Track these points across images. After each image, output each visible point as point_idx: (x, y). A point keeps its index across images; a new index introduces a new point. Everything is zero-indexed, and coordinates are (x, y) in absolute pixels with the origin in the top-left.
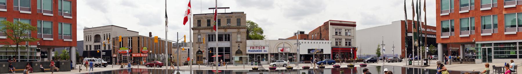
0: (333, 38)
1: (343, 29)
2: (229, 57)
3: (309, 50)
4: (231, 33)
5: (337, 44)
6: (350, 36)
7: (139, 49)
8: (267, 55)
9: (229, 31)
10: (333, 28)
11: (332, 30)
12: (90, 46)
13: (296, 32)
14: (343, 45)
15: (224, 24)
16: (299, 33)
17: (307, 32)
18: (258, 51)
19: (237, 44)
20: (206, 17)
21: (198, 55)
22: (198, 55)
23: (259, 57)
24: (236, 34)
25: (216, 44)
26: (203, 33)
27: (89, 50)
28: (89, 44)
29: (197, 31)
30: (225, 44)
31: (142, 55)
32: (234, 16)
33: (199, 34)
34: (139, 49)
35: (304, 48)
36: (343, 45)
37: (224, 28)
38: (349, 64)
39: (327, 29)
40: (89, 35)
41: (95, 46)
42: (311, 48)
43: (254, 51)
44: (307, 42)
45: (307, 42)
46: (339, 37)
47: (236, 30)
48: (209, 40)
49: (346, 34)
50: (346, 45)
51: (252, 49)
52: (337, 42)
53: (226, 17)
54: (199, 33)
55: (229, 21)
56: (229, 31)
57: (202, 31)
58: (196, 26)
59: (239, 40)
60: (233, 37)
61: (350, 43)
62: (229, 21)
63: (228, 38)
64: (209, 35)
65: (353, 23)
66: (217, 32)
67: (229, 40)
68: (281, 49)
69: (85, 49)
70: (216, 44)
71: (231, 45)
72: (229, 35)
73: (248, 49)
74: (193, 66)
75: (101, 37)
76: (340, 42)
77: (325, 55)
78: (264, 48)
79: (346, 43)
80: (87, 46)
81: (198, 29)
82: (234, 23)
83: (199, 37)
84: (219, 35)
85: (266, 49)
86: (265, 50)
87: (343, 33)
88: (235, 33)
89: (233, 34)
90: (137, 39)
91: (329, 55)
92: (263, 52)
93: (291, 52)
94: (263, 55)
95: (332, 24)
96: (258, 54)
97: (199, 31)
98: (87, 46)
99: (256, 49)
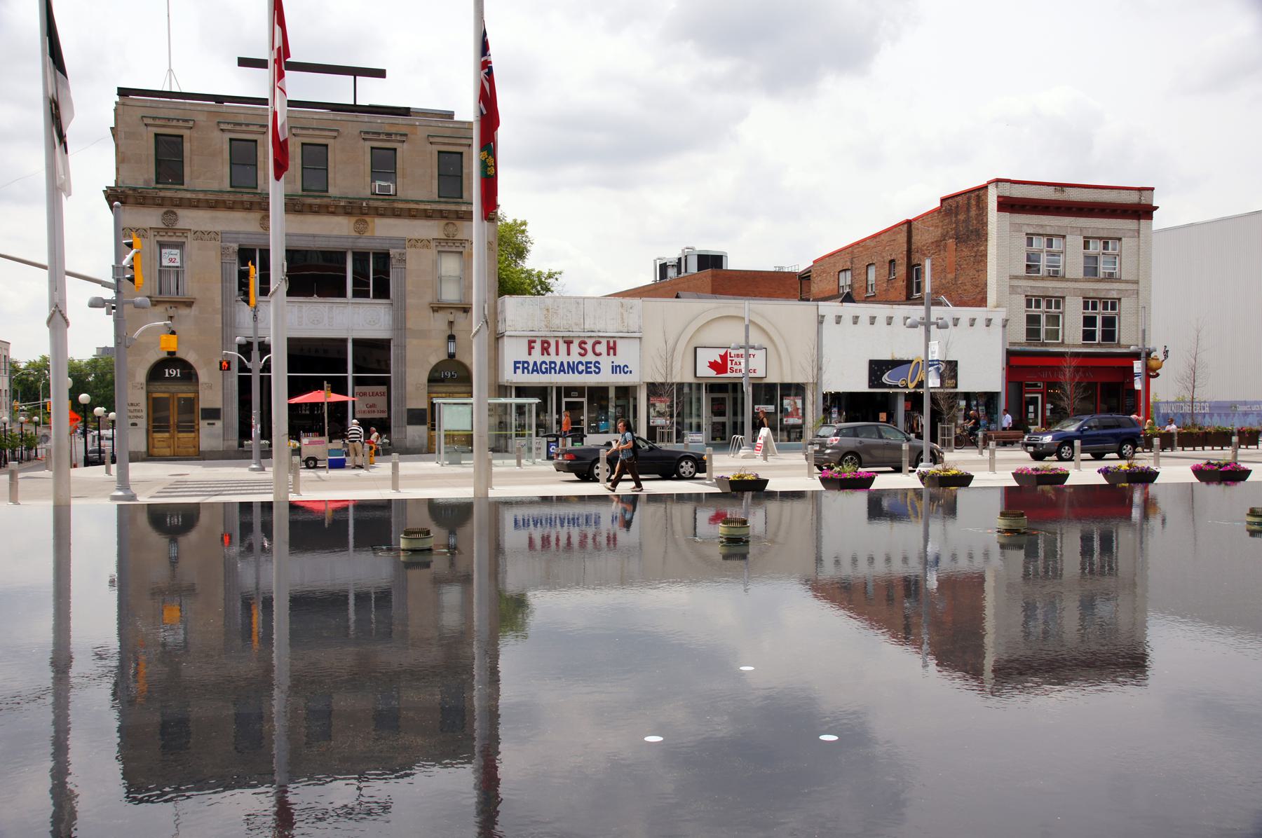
0: (1013, 290)
1: (1072, 243)
2: (381, 402)
3: (877, 368)
4: (403, 242)
5: (1032, 333)
6: (1110, 277)
8: (625, 393)
9: (384, 230)
10: (1016, 228)
11: (1003, 239)
13: (672, 255)
14: (1071, 335)
15: (349, 175)
16: (693, 267)
17: (732, 264)
18: (573, 368)
19: (439, 323)
20: (221, 124)
21: (161, 392)
22: (161, 392)
23: (574, 408)
24: (431, 253)
25: (284, 319)
26: (201, 235)
27: (109, 294)
29: (151, 218)
30: (347, 319)
32: (422, 133)
33: (169, 237)
35: (844, 348)
36: (1071, 335)
37: (353, 208)
38: (1113, 462)
39: (974, 235)
42: (886, 356)
43: (551, 368)
44: (964, 321)
45: (964, 321)
46: (1052, 287)
47: (430, 230)
49: (1091, 270)
50: (1089, 336)
51: (537, 356)
52: (1033, 320)
53: (366, 135)
54: (169, 228)
55: (384, 163)
56: (384, 230)
57: (189, 219)
58: (144, 175)
60: (412, 273)
61: (1109, 322)
62: (384, 163)
63: (375, 275)
64: (245, 255)
65: (1132, 198)
66: (280, 232)
67: (382, 291)
68: (715, 356)
70: (284, 319)
71: (400, 323)
72: (383, 259)
73: (513, 351)
74: (138, 471)
76: (1054, 319)
77: (967, 396)
78: (612, 349)
79: (1090, 321)
81: (159, 202)
82: (417, 179)
83: (171, 257)
84: (291, 254)
85: (627, 353)
86: (619, 360)
87: (1073, 263)
88: (425, 243)
89: (410, 253)
91: (991, 398)
92: (605, 377)
93: (773, 378)
94: (598, 394)
95: (1007, 205)
96: (569, 390)
97: (170, 216)
99: (563, 358)
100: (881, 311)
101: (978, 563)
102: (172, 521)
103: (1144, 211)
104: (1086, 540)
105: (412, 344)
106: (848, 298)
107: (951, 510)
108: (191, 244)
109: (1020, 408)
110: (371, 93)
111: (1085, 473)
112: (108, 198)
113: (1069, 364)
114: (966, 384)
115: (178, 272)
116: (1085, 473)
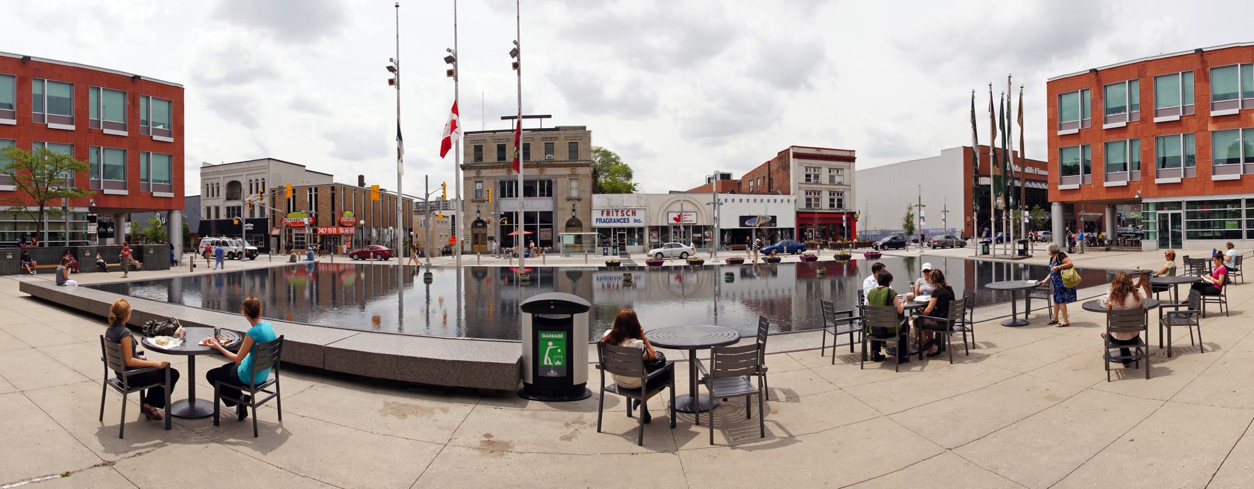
1: (824, 168)
2: (549, 234)
3: (743, 219)
4: (556, 176)
6: (840, 184)
7: (333, 215)
8: (641, 230)
9: (550, 172)
10: (801, 165)
11: (797, 170)
12: (217, 209)
13: (712, 174)
14: (825, 205)
15: (537, 154)
16: (719, 178)
17: (737, 176)
18: (619, 221)
19: (569, 205)
20: (494, 140)
21: (476, 231)
22: (476, 231)
23: (622, 236)
25: (519, 204)
26: (488, 178)
28: (213, 203)
29: (473, 173)
30: (540, 204)
31: (341, 230)
33: (479, 180)
34: (333, 215)
35: (730, 213)
36: (825, 205)
37: (539, 165)
38: (838, 252)
39: (786, 167)
40: (215, 182)
41: (228, 208)
43: (610, 221)
46: (816, 187)
48: (503, 195)
49: (832, 179)
50: (832, 206)
51: (605, 217)
52: (808, 200)
53: (543, 139)
55: (549, 148)
56: (550, 172)
57: (484, 173)
58: (471, 159)
59: (574, 194)
60: (560, 187)
61: (840, 201)
62: (549, 148)
63: (547, 189)
64: (502, 183)
65: (847, 154)
66: (521, 176)
67: (550, 194)
68: (676, 215)
69: (204, 216)
70: (519, 204)
71: (555, 205)
72: (550, 182)
73: (596, 215)
75: (244, 186)
77: (782, 229)
78: (634, 213)
79: (832, 200)
80: (209, 209)
81: (475, 168)
82: (562, 154)
83: (479, 186)
85: (640, 215)
87: (824, 177)
89: (559, 180)
90: (329, 191)
92: (631, 224)
94: (631, 231)
95: (796, 156)
96: (620, 229)
97: (478, 172)
98: (209, 209)
99: (615, 217)
100: (759, 197)
101: (787, 293)
102: (478, 273)
103: (851, 159)
104: (833, 285)
105: (560, 213)
106: (752, 193)
107: (775, 274)
108: (485, 181)
109: (802, 236)
110: (547, 124)
111: (826, 255)
112: (134, 88)
113: (817, 217)
114: (779, 225)
115: (481, 191)
116: (826, 255)
